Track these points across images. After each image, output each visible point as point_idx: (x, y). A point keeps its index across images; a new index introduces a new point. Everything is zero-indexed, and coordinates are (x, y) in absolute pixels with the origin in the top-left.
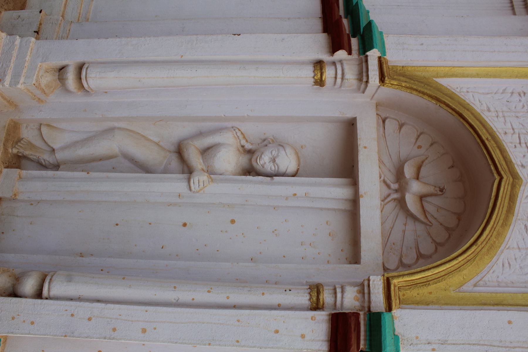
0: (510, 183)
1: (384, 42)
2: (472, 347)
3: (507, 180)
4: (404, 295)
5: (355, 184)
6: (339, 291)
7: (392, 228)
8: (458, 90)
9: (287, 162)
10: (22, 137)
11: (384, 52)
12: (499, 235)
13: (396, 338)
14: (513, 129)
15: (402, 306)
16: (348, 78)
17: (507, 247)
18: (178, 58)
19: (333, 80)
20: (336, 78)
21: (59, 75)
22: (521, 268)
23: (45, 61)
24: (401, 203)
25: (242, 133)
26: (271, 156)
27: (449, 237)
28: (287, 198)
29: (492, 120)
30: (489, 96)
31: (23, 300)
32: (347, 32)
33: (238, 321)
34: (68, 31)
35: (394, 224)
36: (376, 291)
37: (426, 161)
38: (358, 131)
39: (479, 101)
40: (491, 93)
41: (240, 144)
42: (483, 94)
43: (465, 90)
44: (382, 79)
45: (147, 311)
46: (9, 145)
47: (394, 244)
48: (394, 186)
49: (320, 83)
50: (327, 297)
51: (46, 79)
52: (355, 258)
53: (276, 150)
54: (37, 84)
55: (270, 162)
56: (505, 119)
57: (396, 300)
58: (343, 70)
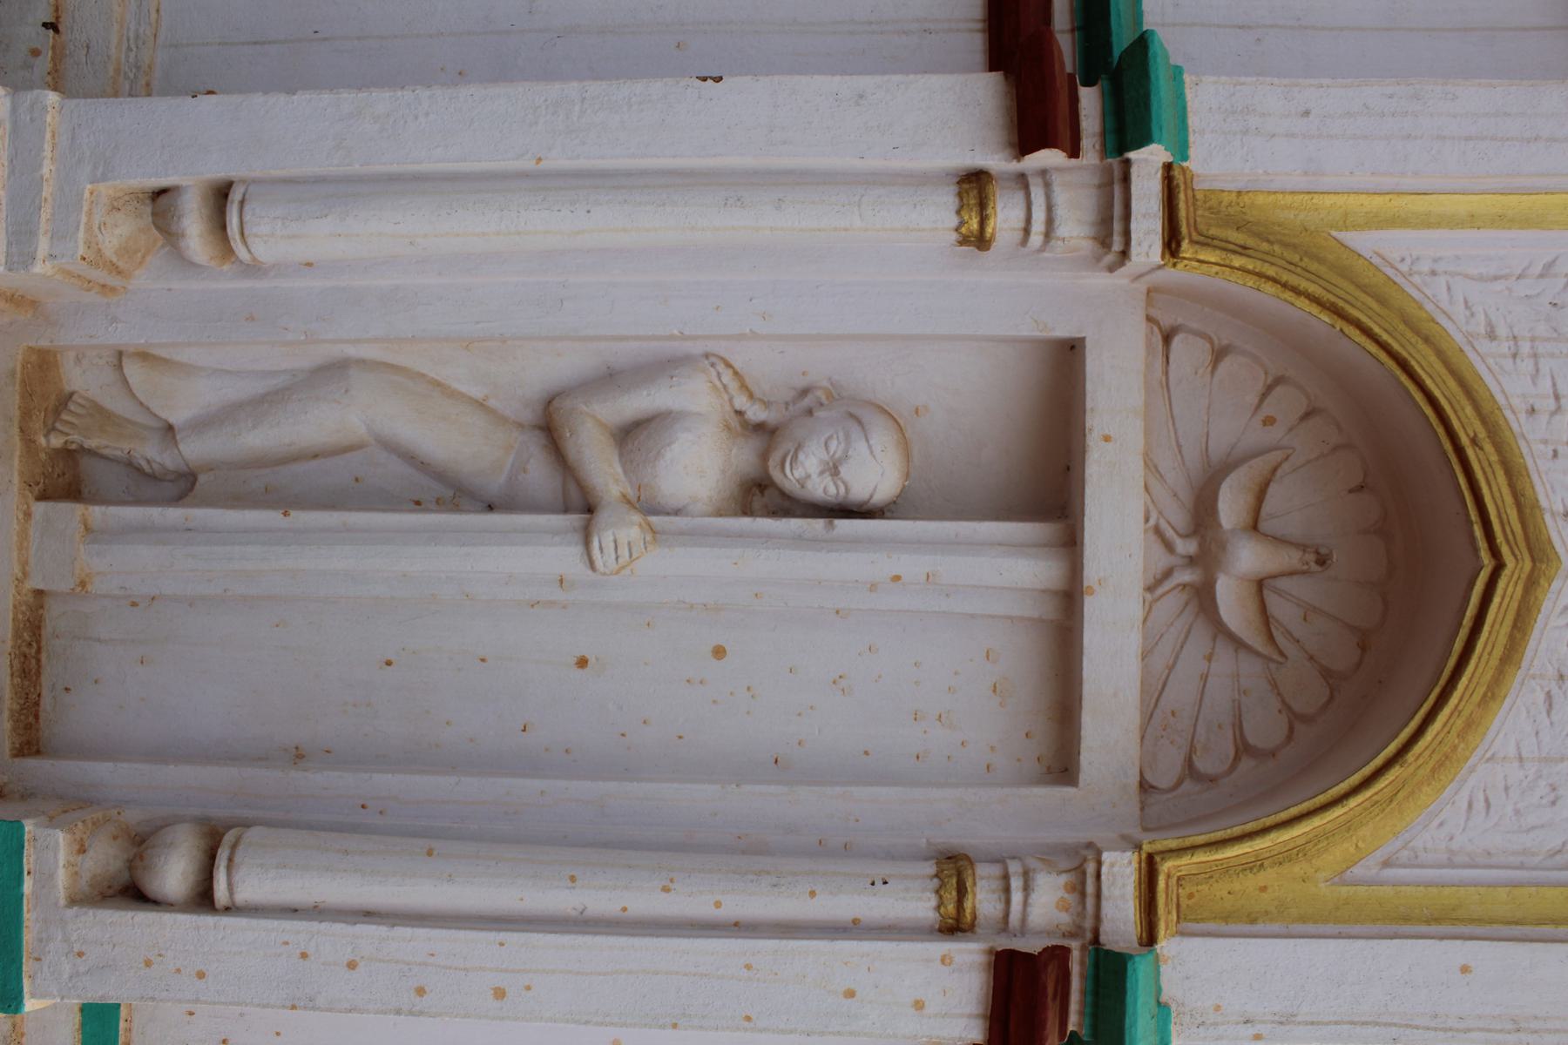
0: (1524, 576)
1: (1184, 108)
2: (1358, 1028)
3: (1515, 569)
4: (1191, 896)
5: (1071, 543)
6: (1016, 884)
7: (1171, 668)
8: (1404, 268)
9: (873, 472)
10: (68, 389)
11: (1182, 149)
12: (1470, 725)
13: (1162, 1007)
14: (1557, 397)
15: (1184, 925)
16: (1066, 235)
17: (1488, 755)
18: (528, 164)
19: (1019, 235)
20: (1027, 231)
21: (154, 214)
22: (1517, 812)
23: (104, 178)
24: (1203, 598)
25: (736, 373)
26: (826, 457)
27: (1332, 698)
28: (873, 587)
29: (1495, 368)
30: (1499, 286)
31: (167, 918)
32: (1069, 69)
33: (748, 967)
34: (154, 15)
35: (1177, 657)
36: (1117, 893)
37: (1286, 467)
38: (1089, 386)
39: (1466, 302)
40: (1505, 277)
41: (732, 405)
42: (1481, 278)
43: (1425, 267)
44: (1172, 243)
45: (502, 944)
46: (37, 425)
47: (1173, 714)
48: (1187, 547)
49: (980, 241)
50: (984, 901)
51: (117, 231)
52: (1062, 766)
53: (841, 434)
54: (90, 255)
55: (821, 473)
56: (1536, 364)
57: (1169, 913)
58: (1050, 208)
